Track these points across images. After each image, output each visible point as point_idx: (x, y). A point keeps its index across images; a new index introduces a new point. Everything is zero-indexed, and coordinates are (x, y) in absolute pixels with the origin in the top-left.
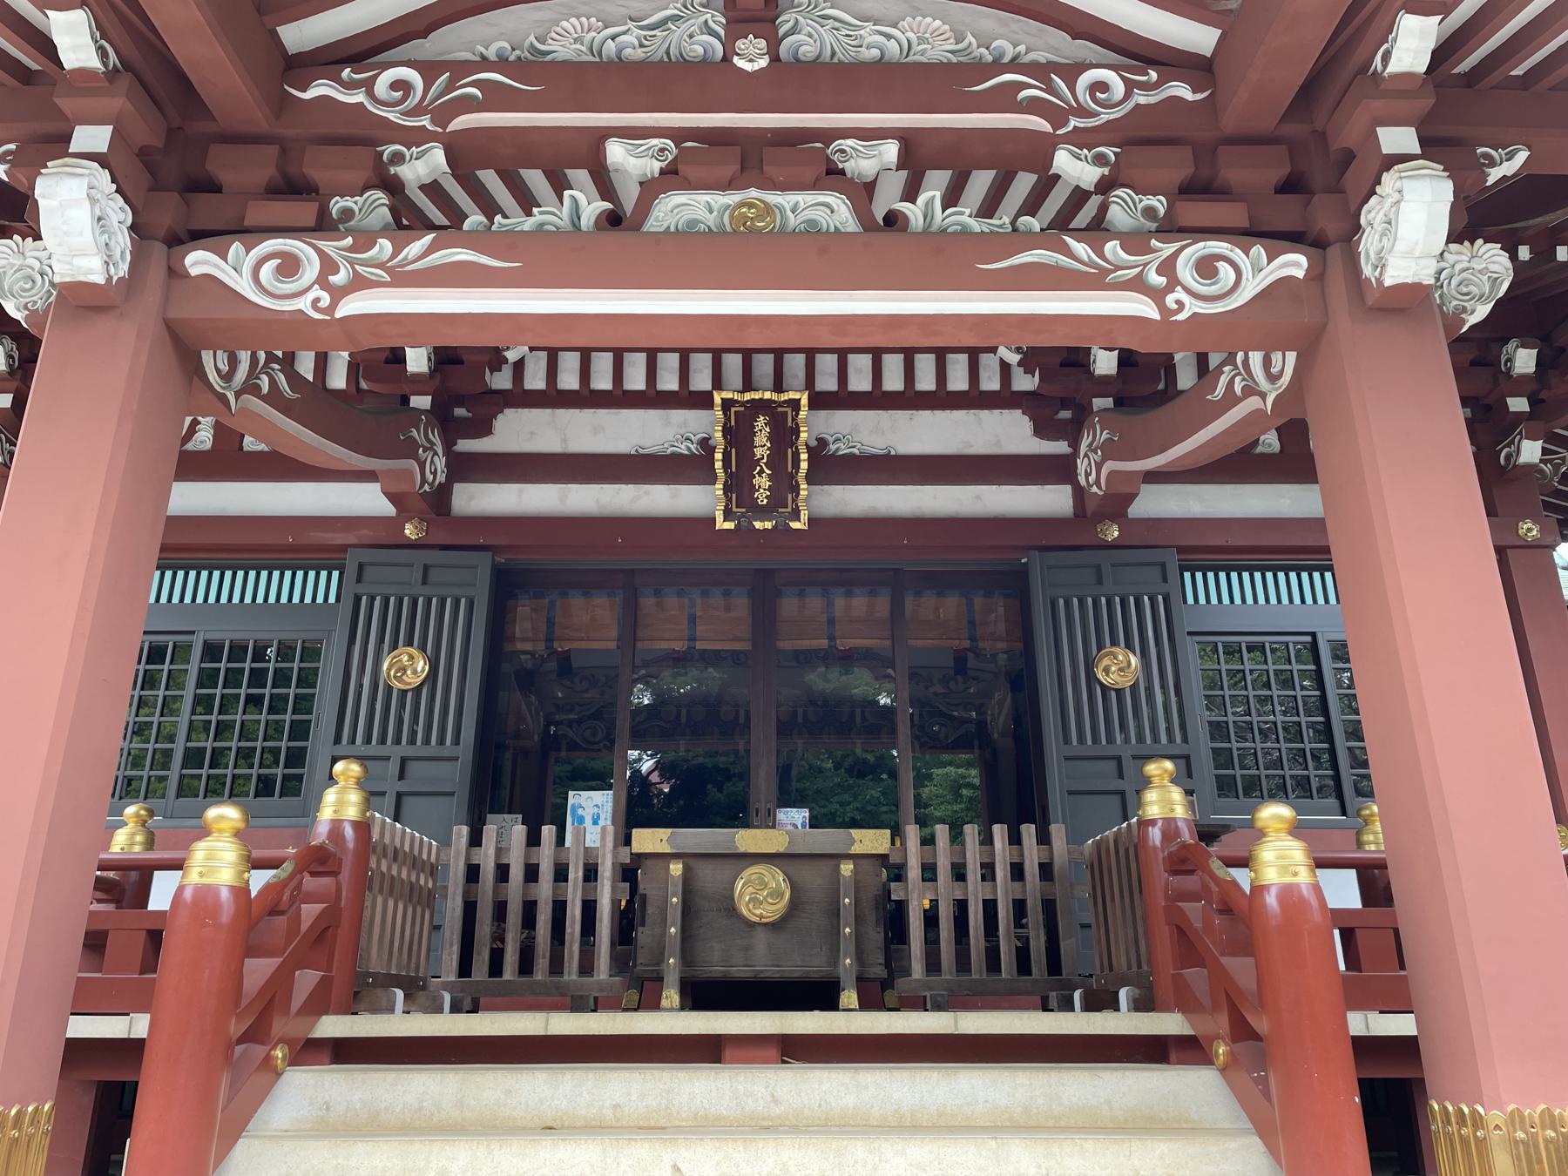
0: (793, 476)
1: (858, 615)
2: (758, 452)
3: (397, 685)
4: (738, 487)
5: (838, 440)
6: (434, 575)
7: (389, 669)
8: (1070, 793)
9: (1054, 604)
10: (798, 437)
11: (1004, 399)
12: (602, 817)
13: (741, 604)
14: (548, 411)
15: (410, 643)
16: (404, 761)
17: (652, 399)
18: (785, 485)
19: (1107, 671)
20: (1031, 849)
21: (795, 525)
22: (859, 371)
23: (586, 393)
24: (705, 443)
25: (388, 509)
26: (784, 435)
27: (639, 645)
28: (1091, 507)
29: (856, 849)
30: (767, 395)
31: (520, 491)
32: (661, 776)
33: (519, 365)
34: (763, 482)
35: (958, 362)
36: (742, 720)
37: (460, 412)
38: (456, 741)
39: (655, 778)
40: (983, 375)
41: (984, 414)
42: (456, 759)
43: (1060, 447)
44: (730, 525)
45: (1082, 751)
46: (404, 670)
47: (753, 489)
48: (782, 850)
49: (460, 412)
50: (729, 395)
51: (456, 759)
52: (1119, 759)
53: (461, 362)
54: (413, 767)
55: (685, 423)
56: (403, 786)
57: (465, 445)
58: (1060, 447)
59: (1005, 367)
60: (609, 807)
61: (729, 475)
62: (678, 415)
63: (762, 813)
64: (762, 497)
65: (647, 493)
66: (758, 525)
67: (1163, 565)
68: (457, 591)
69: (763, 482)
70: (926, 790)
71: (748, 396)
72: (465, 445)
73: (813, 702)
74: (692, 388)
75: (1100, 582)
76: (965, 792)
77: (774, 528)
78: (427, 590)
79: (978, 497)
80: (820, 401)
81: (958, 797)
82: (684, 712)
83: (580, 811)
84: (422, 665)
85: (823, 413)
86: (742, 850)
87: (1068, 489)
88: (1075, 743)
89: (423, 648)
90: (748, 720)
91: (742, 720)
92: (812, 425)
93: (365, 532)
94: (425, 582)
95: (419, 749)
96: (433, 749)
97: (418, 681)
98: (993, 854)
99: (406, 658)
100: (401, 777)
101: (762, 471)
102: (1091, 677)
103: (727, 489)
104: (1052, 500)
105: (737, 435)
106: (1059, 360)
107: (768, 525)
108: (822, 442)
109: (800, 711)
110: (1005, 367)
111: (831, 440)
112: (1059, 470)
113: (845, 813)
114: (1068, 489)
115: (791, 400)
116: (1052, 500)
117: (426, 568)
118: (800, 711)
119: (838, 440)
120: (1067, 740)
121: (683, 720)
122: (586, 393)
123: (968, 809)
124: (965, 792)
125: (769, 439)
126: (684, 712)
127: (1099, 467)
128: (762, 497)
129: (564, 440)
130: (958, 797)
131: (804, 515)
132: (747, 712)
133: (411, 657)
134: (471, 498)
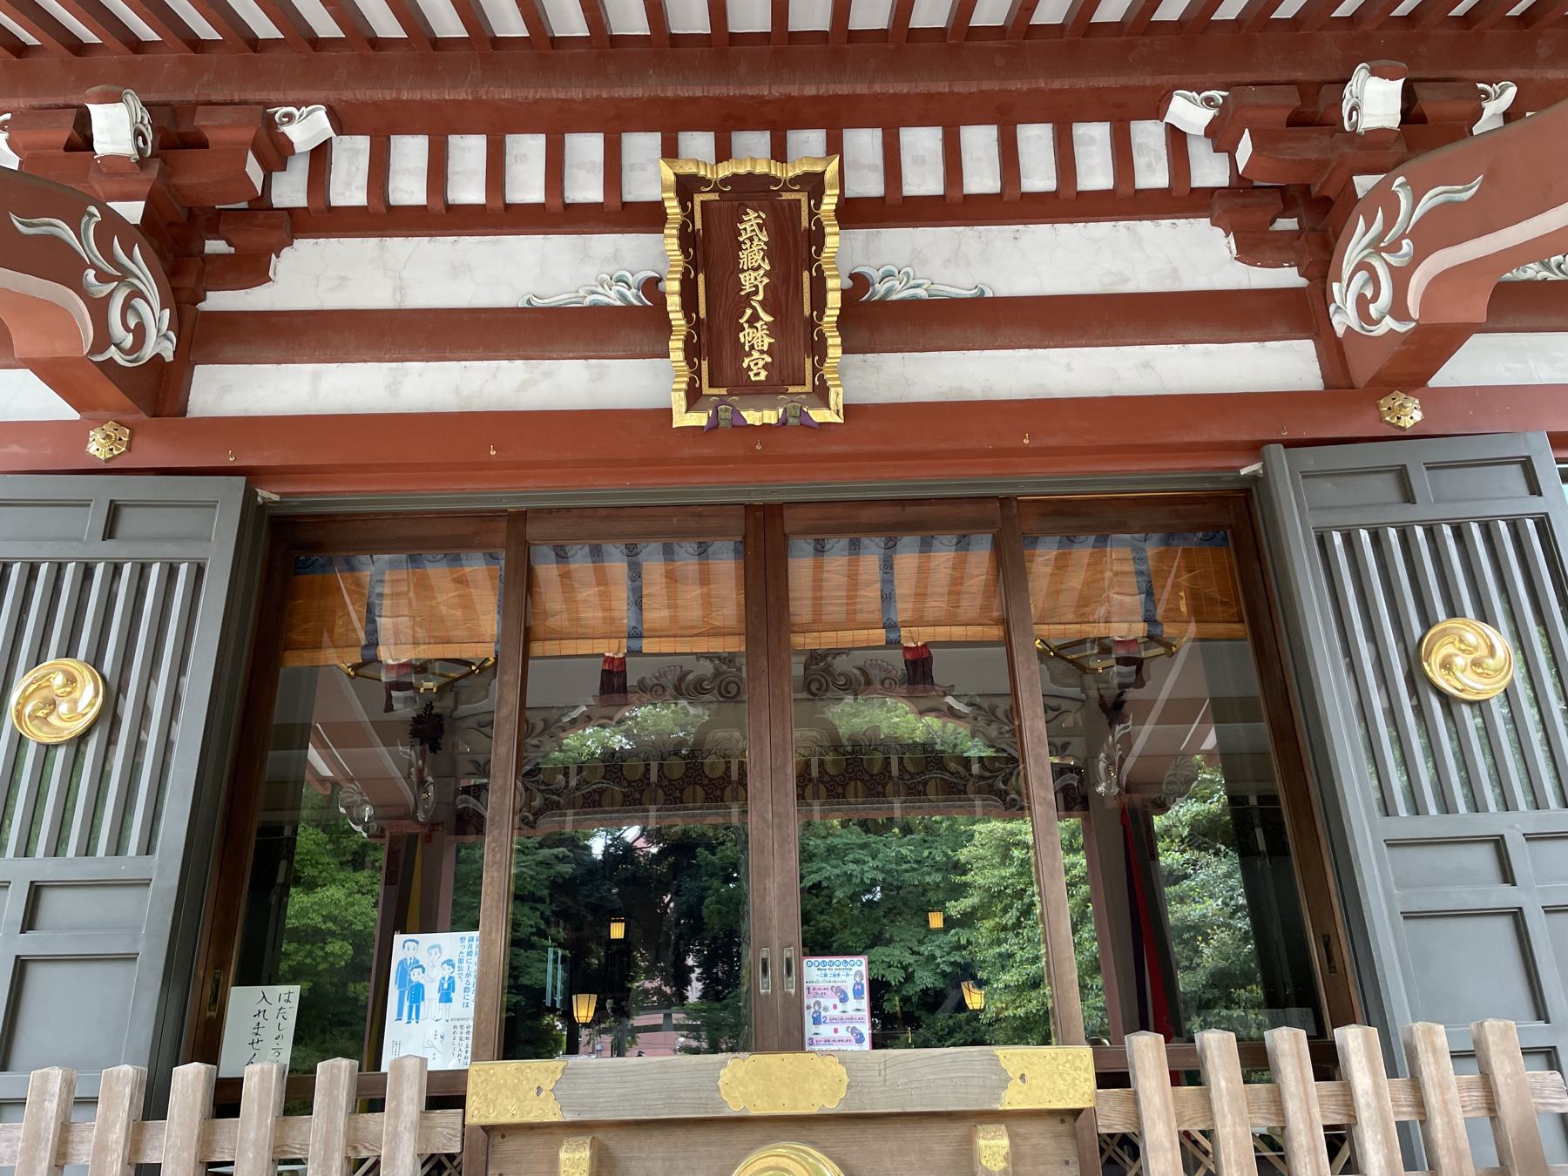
0: (812, 324)
1: (932, 587)
2: (748, 280)
3: (37, 735)
4: (712, 348)
5: (888, 275)
6: (130, 521)
7: (25, 699)
8: (1408, 916)
9: (1323, 542)
10: (821, 246)
11: (1181, 200)
12: (459, 986)
13: (726, 566)
14: (373, 241)
15: (69, 650)
16: (35, 891)
17: (556, 216)
18: (799, 340)
19: (1446, 665)
20: (1443, 1087)
21: (819, 416)
22: (920, 161)
23: (439, 206)
24: (652, 287)
25: (57, 408)
26: (796, 248)
27: (537, 648)
28: (1363, 370)
29: (1014, 1099)
30: (761, 169)
31: (317, 377)
32: (648, 841)
33: (320, 156)
34: (757, 338)
35: (1092, 140)
36: (734, 776)
37: (215, 246)
38: (148, 848)
39: (641, 843)
40: (1139, 161)
41: (1145, 227)
42: (145, 883)
43: (1287, 277)
44: (699, 419)
45: (1433, 822)
46: (52, 704)
47: (740, 351)
48: (832, 1107)
49: (215, 246)
50: (690, 169)
51: (145, 883)
52: (1499, 844)
53: (204, 145)
54: (53, 903)
55: (616, 257)
56: (29, 944)
57: (218, 301)
58: (1287, 277)
59: (1177, 139)
60: (472, 965)
61: (695, 326)
62: (605, 244)
63: (776, 968)
64: (757, 366)
65: (548, 375)
66: (752, 417)
67: (1527, 466)
68: (171, 551)
69: (757, 338)
70: (965, 851)
71: (725, 170)
72: (218, 301)
73: (836, 746)
74: (628, 197)
75: (1408, 497)
76: (1016, 853)
77: (783, 423)
78: (112, 549)
79: (1146, 365)
80: (855, 213)
81: (1006, 858)
82: (654, 766)
83: (416, 976)
84: (87, 698)
85: (860, 235)
86: (734, 1108)
87: (1308, 346)
88: (1403, 812)
89: (96, 661)
90: (743, 774)
91: (734, 776)
92: (845, 252)
93: (15, 448)
94: (109, 533)
95: (70, 865)
96: (101, 864)
97: (79, 726)
98: (1348, 1100)
99: (59, 680)
100: (29, 923)
101: (755, 318)
102: (1416, 678)
103: (691, 352)
104: (1287, 365)
105: (707, 251)
106: (1284, 115)
107: (771, 417)
108: (860, 282)
109: (814, 761)
110: (1177, 139)
111: (876, 276)
112: (1301, 313)
113: (863, 872)
114: (1308, 346)
115: (807, 175)
116: (1287, 365)
117: (114, 510)
118: (814, 761)
119: (888, 275)
120: (1387, 808)
121: (654, 777)
122: (439, 206)
123: (1021, 874)
124: (1016, 853)
125: (768, 254)
126: (654, 766)
127: (1400, 278)
128: (757, 366)
129: (400, 289)
130: (1006, 858)
131: (837, 397)
132: (742, 765)
133: (71, 680)
134: (226, 389)
